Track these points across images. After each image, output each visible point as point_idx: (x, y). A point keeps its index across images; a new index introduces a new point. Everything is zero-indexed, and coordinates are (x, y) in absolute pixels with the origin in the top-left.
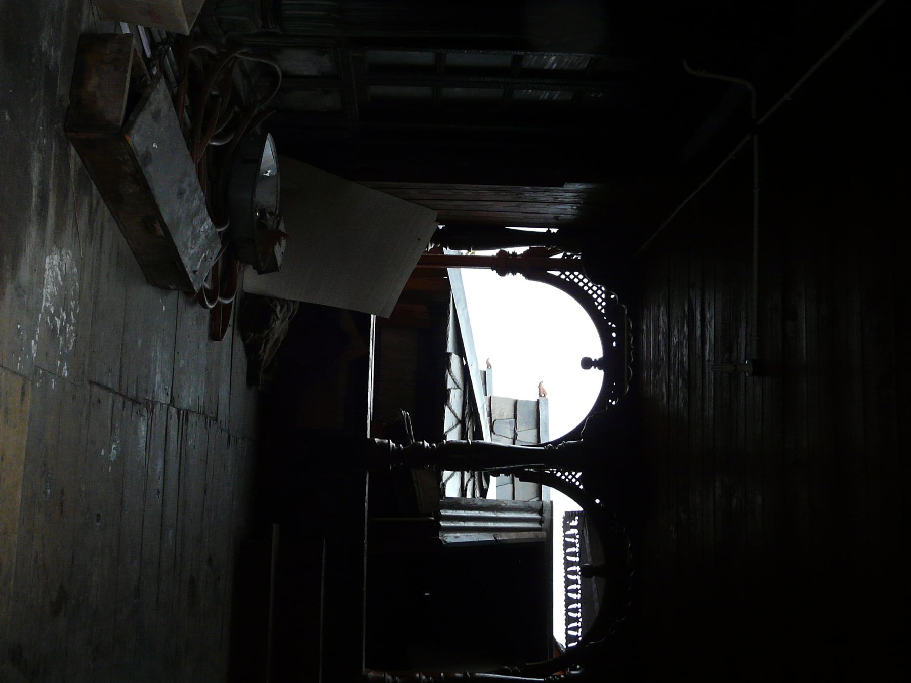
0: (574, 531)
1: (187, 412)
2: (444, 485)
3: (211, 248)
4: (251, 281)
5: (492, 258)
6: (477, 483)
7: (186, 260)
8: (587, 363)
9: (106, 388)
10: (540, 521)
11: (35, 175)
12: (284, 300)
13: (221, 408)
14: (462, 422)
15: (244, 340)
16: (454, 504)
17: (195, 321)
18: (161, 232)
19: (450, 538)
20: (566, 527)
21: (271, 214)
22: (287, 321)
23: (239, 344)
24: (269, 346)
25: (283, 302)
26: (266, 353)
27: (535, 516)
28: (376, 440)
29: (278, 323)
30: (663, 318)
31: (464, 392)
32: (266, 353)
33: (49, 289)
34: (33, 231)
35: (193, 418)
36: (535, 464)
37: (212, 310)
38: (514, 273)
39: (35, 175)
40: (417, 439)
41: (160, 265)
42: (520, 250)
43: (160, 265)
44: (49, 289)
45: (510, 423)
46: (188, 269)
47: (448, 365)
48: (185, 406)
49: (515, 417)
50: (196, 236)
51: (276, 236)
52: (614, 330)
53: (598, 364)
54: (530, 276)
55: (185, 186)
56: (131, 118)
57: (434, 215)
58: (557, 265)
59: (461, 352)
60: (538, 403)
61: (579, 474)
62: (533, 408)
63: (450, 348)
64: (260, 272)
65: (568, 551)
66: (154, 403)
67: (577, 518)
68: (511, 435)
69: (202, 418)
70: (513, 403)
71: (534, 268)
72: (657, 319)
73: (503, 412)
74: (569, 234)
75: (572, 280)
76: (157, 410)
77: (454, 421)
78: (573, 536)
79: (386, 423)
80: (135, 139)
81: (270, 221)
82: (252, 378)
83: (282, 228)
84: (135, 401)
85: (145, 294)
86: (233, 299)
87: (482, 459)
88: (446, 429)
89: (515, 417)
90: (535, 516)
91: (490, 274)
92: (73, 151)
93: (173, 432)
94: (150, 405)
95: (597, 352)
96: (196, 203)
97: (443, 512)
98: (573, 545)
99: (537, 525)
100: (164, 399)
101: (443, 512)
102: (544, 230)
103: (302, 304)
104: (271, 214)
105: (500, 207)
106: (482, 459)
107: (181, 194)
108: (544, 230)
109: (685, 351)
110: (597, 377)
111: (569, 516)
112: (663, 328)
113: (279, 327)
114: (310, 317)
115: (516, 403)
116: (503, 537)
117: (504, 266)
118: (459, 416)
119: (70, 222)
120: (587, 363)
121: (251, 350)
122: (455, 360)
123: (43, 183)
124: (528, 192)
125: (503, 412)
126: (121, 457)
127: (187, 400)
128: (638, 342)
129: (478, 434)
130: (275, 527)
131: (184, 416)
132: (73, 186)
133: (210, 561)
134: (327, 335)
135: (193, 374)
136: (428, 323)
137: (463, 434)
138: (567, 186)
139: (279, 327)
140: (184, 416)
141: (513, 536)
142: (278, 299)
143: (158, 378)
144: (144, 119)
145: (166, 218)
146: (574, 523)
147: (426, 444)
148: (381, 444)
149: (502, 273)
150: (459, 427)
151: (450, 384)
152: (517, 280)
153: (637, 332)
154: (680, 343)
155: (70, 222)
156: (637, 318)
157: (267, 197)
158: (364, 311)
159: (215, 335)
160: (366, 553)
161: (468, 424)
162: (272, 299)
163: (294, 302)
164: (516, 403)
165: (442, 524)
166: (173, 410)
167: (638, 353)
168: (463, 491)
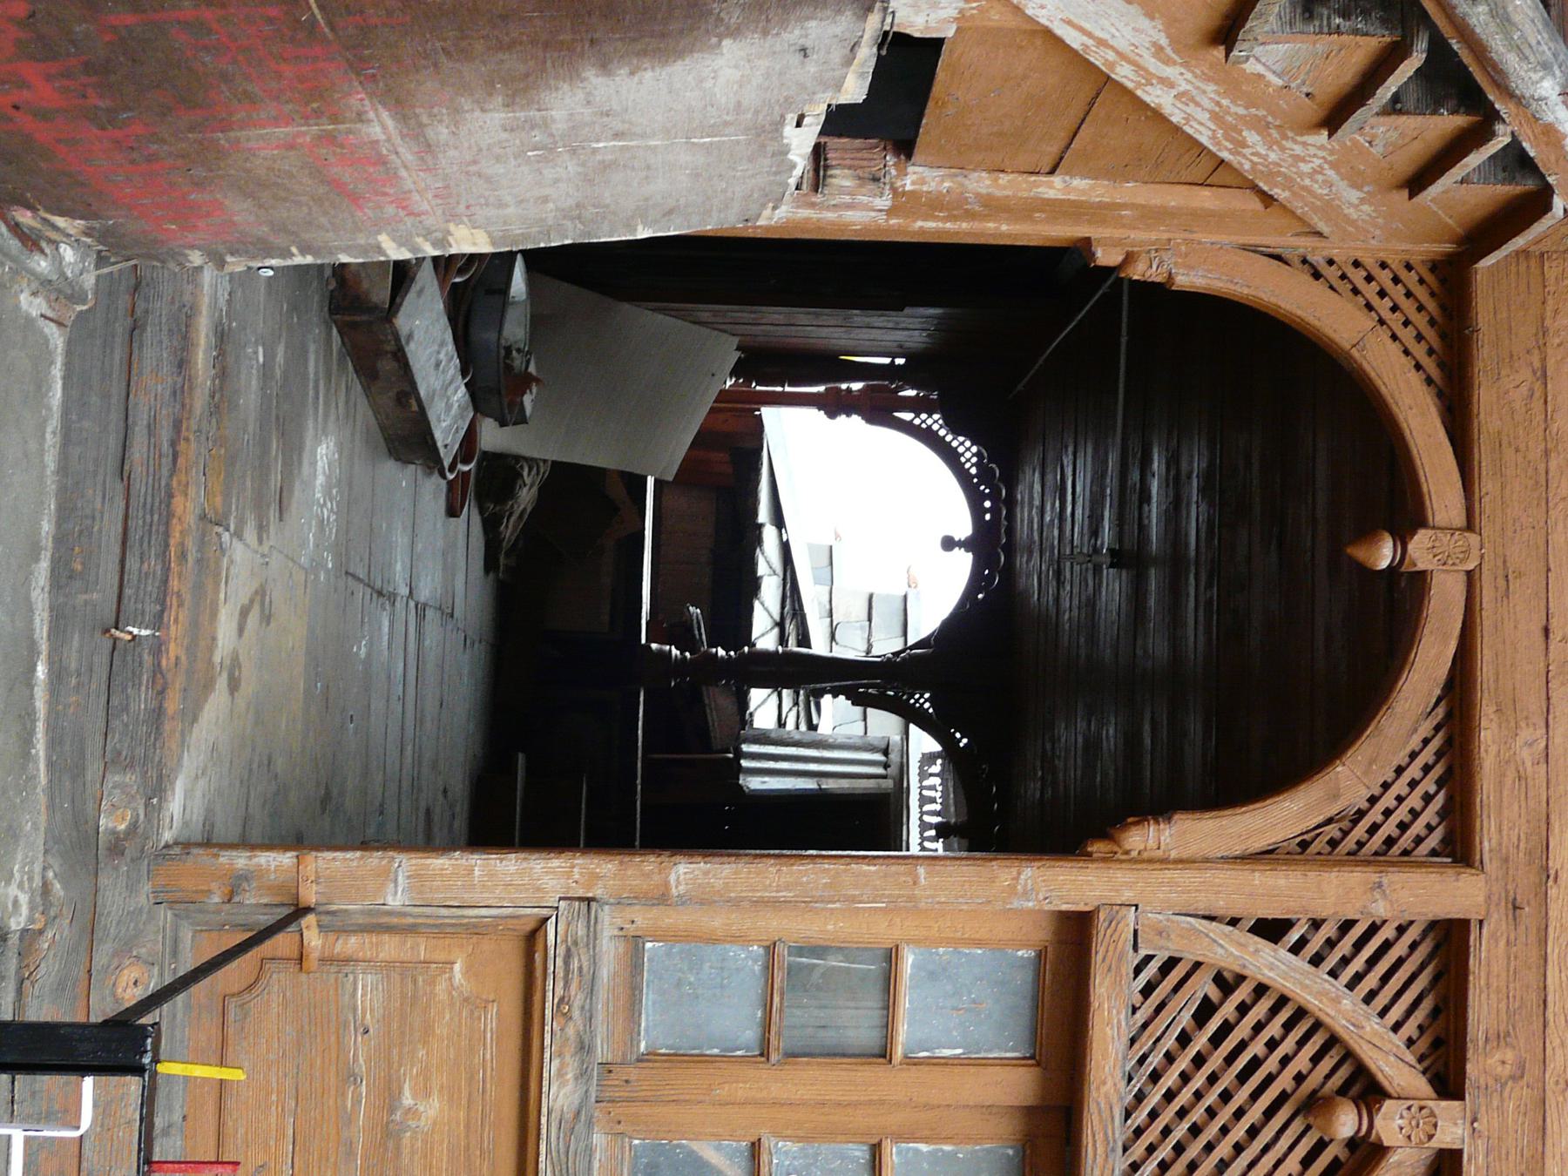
0: (936, 781)
1: (425, 605)
2: (751, 715)
3: (462, 417)
4: (492, 437)
5: (818, 394)
6: (802, 714)
7: (438, 435)
8: (949, 544)
9: (358, 579)
10: (886, 766)
11: (311, 369)
12: (533, 459)
13: (457, 600)
14: (780, 625)
15: (481, 513)
16: (763, 738)
17: (433, 491)
18: (415, 407)
19: (755, 783)
20: (923, 775)
21: (519, 351)
22: (535, 489)
23: (476, 520)
24: (513, 519)
25: (532, 462)
26: (508, 530)
27: (879, 757)
28: (654, 646)
29: (525, 490)
30: (1037, 487)
31: (784, 579)
32: (509, 530)
33: (320, 479)
34: (310, 424)
35: (430, 613)
36: (866, 682)
37: (450, 483)
38: (848, 415)
39: (311, 369)
40: (711, 645)
41: (408, 438)
42: (857, 386)
43: (408, 438)
44: (320, 479)
45: (862, 628)
46: (440, 444)
47: (758, 541)
48: (422, 599)
49: (870, 620)
50: (449, 407)
51: (525, 381)
52: (986, 497)
53: (967, 545)
54: (870, 420)
55: (442, 356)
56: (398, 300)
57: (735, 341)
58: (908, 404)
59: (779, 522)
60: (905, 597)
61: (927, 695)
62: (899, 605)
63: (763, 515)
64: (503, 424)
65: (927, 808)
66: (395, 595)
67: (939, 761)
68: (865, 647)
69: (439, 614)
70: (866, 598)
71: (878, 410)
72: (1031, 487)
73: (850, 609)
74: (919, 367)
75: (929, 427)
76: (398, 604)
77: (769, 623)
78: (933, 788)
79: (670, 626)
80: (402, 322)
81: (517, 361)
82: (490, 564)
83: (532, 369)
84: (380, 594)
85: (390, 467)
86: (472, 465)
87: (807, 675)
88: (754, 636)
89: (870, 620)
90: (879, 757)
91: (814, 415)
92: (335, 331)
93: (412, 629)
94: (392, 598)
95: (963, 527)
96: (451, 372)
97: (745, 748)
98: (933, 800)
99: (880, 771)
100: (404, 591)
101: (745, 748)
102: (887, 361)
103: (554, 462)
104: (519, 351)
105: (824, 332)
106: (807, 675)
107: (438, 365)
108: (887, 361)
109: (1056, 533)
110: (962, 564)
111: (929, 759)
112: (1037, 502)
113: (526, 496)
114: (568, 482)
115: (871, 597)
116: (829, 784)
117: (834, 405)
118: (777, 618)
119: (333, 410)
120: (949, 544)
121: (491, 526)
122: (769, 534)
123: (316, 373)
124: (858, 317)
125: (850, 609)
126: (369, 655)
127: (424, 594)
128: (1011, 517)
129: (804, 640)
130: (521, 756)
131: (421, 610)
132: (335, 367)
133: (445, 791)
134: (585, 505)
135: (434, 557)
136: (727, 478)
137: (783, 640)
138: (908, 311)
139: (526, 496)
140: (421, 610)
141: (845, 784)
142: (526, 459)
143: (399, 567)
144: (410, 301)
145: (422, 393)
146: (936, 769)
147: (721, 652)
148: (660, 652)
149: (832, 415)
150: (776, 630)
151: (762, 569)
152: (853, 425)
153: (1011, 502)
154: (1052, 521)
155: (333, 410)
156: (1011, 480)
157: (515, 329)
158: (638, 472)
159: (452, 512)
160: (639, 796)
161: (791, 628)
162: (518, 458)
163: (545, 461)
164: (871, 597)
165: (744, 763)
166: (412, 604)
167: (1010, 531)
168: (781, 724)
